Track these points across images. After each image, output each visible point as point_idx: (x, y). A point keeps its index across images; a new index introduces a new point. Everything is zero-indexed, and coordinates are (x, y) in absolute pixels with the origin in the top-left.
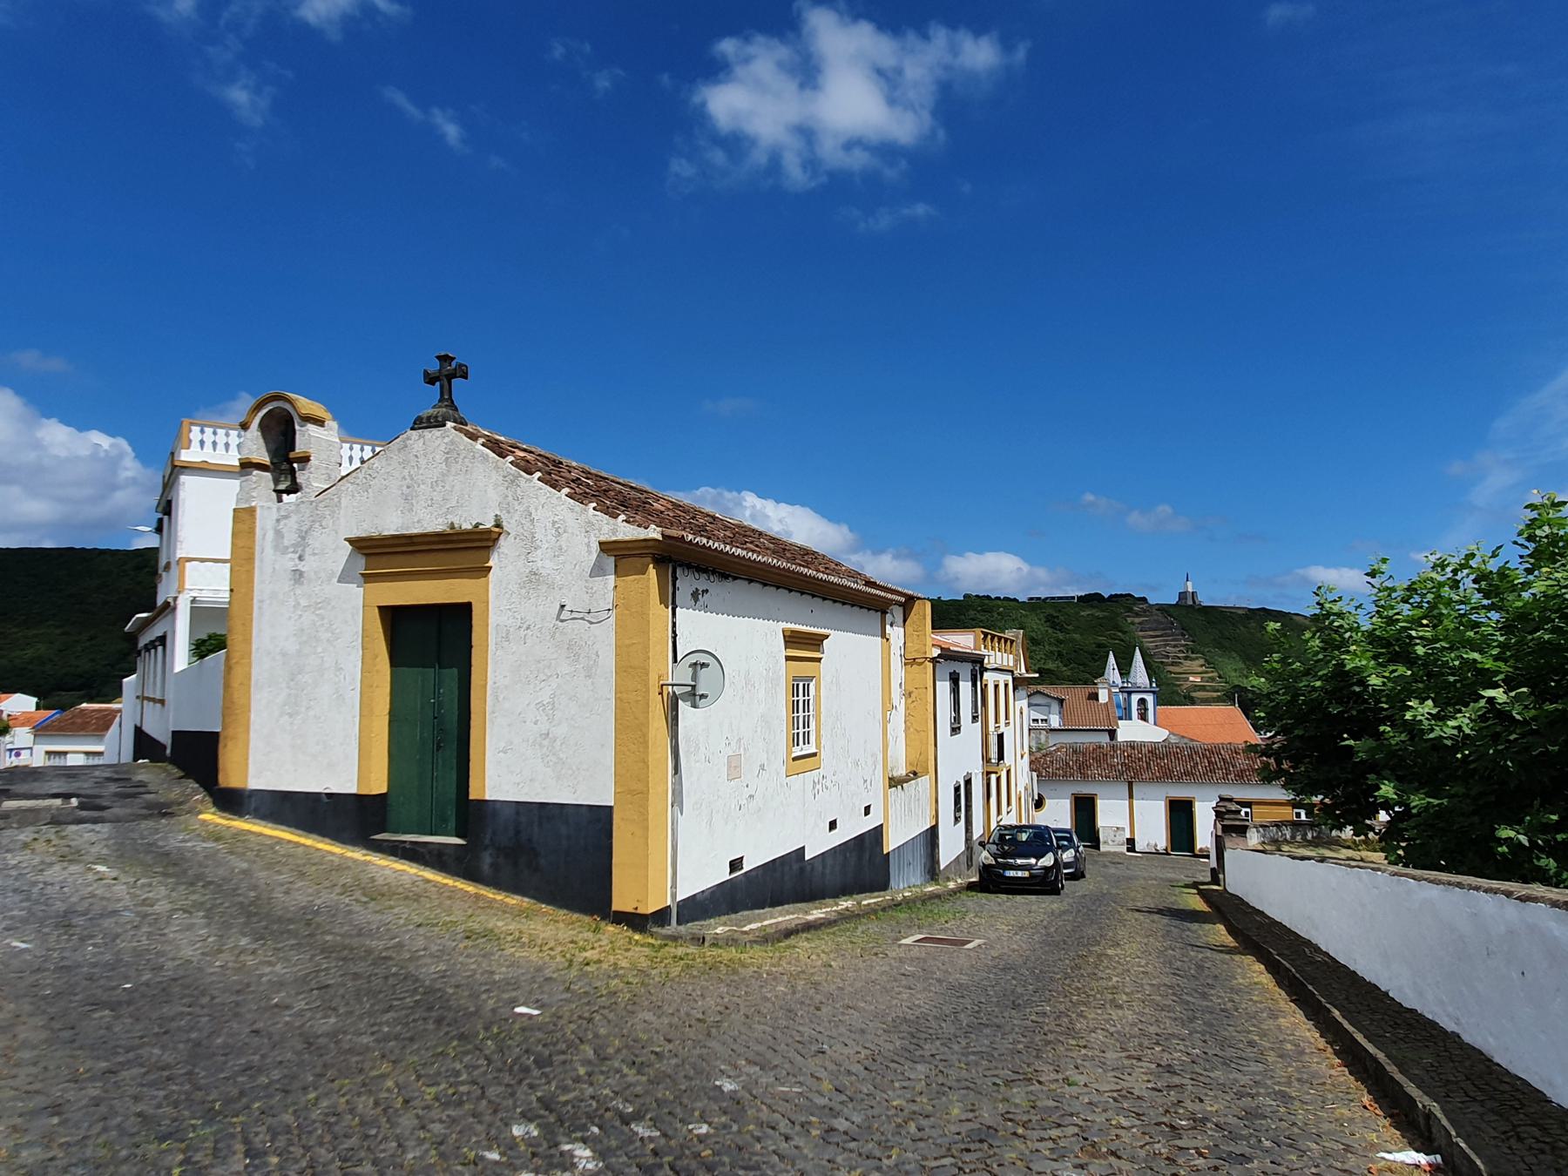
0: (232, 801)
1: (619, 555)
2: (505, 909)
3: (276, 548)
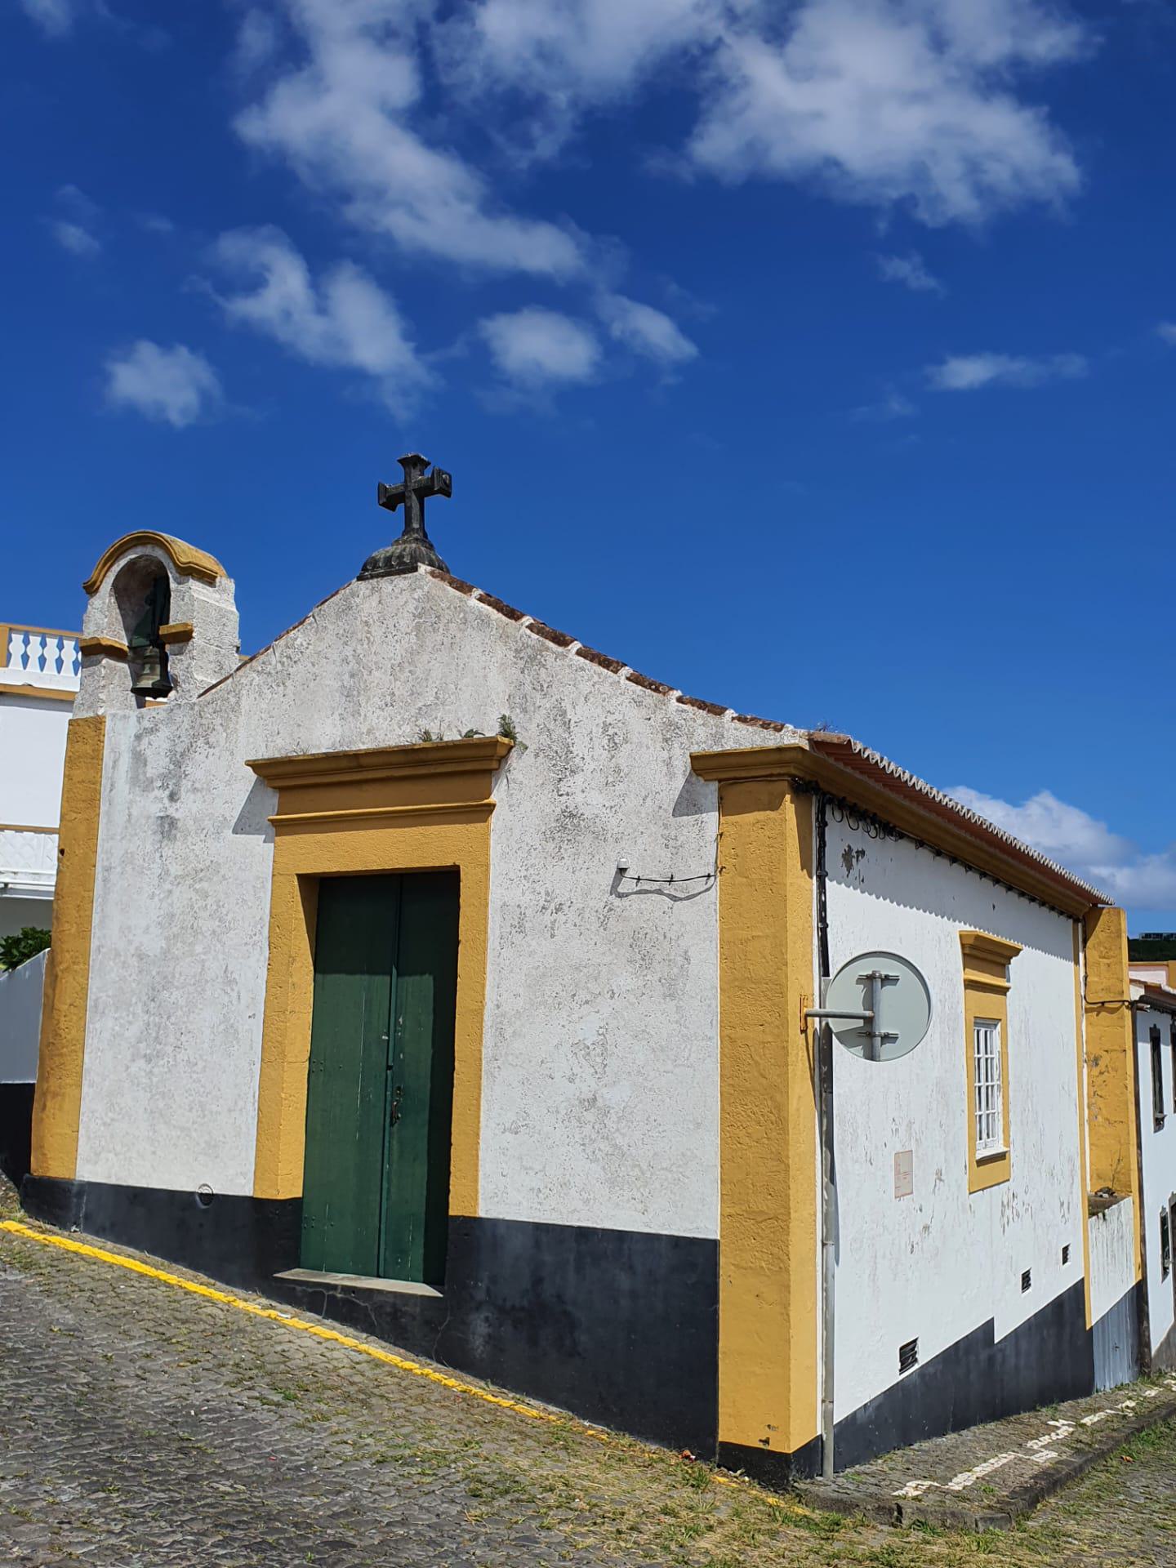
0: (51, 1201)
1: (726, 778)
2: (522, 1430)
3: (134, 780)
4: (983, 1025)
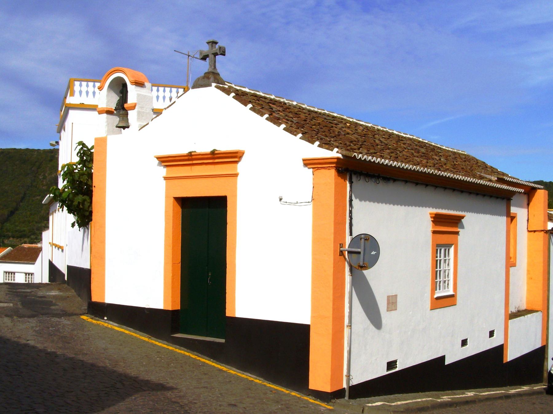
4: (439, 246)
